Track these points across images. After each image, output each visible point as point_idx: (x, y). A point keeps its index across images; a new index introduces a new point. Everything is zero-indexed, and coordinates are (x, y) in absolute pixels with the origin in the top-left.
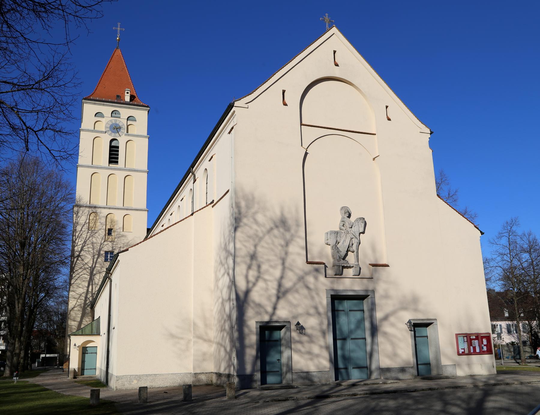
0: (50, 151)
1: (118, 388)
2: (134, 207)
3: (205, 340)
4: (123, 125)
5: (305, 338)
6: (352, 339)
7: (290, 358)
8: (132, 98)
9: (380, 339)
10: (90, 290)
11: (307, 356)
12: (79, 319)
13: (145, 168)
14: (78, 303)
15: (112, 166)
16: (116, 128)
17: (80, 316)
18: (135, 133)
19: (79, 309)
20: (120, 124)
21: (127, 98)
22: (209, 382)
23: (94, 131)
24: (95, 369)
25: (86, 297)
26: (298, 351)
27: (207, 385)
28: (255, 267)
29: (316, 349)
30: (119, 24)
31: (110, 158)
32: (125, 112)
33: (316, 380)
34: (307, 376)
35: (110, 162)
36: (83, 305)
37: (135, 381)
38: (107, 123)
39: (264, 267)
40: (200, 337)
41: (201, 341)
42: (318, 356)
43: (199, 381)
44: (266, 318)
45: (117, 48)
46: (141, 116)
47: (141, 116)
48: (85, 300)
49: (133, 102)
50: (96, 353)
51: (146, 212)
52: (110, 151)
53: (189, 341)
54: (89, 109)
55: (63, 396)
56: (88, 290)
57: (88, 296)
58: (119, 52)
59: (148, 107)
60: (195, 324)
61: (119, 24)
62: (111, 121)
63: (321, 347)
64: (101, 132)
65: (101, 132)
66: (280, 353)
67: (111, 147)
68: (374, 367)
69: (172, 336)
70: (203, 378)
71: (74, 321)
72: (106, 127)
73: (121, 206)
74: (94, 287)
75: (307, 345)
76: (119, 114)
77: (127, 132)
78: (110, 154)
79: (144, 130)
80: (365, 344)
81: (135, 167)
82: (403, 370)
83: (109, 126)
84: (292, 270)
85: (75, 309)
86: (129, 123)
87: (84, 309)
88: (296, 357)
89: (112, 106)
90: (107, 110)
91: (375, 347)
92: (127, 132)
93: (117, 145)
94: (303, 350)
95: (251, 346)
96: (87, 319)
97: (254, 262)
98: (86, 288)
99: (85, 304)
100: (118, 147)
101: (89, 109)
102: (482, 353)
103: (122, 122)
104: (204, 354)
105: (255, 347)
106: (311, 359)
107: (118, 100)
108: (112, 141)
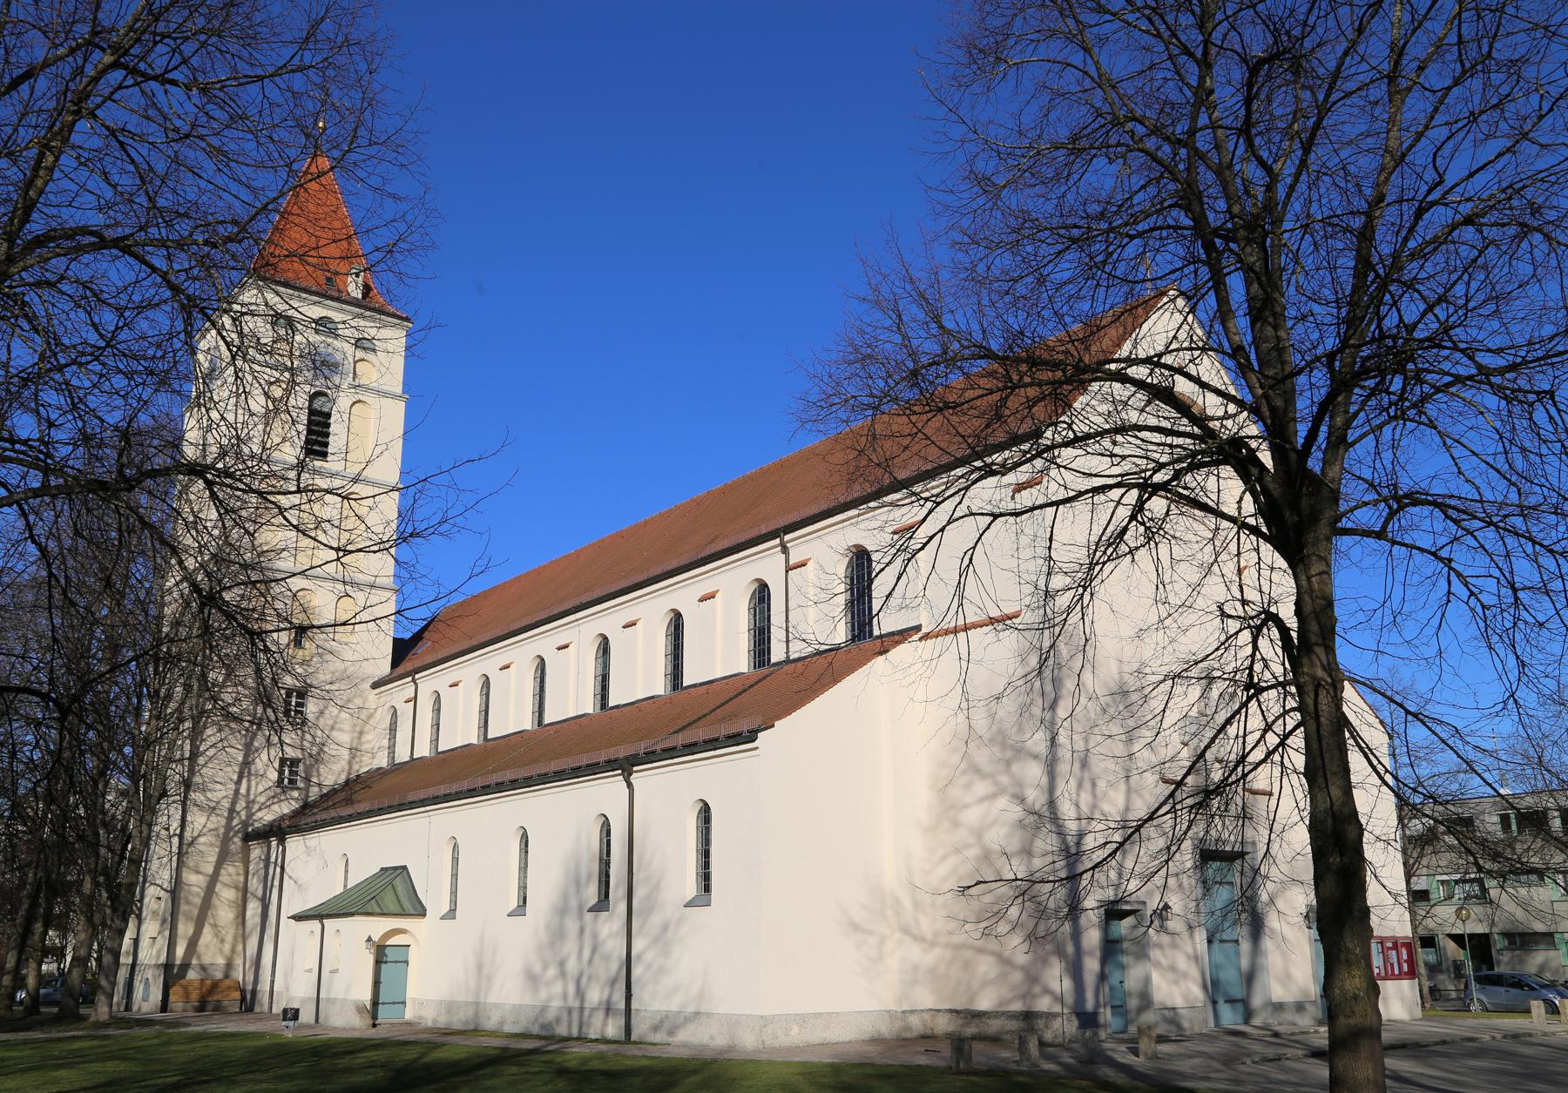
0: (1434, 554)
1: (768, 1043)
3: (915, 938)
5: (1165, 939)
6: (1222, 941)
7: (1147, 981)
9: (1267, 944)
10: (243, 790)
11: (1170, 976)
12: (210, 869)
14: (210, 826)
17: (213, 859)
19: (213, 840)
20: (338, 357)
22: (929, 1032)
24: (404, 1003)
25: (232, 811)
26: (1158, 964)
27: (924, 1037)
28: (1087, 785)
29: (1182, 963)
33: (1186, 1024)
34: (1171, 1016)
36: (222, 830)
37: (796, 1029)
39: (1101, 784)
40: (906, 931)
41: (908, 939)
42: (1185, 975)
43: (907, 1028)
44: (1110, 894)
46: (393, 339)
47: (393, 339)
48: (230, 819)
49: (366, 303)
50: (406, 962)
53: (883, 940)
55: (349, 1070)
56: (237, 792)
57: (238, 808)
59: (407, 319)
60: (897, 901)
63: (1189, 957)
66: (1122, 967)
68: (1257, 1001)
69: (855, 927)
70: (914, 1021)
71: (198, 872)
74: (253, 783)
75: (1168, 951)
79: (395, 384)
80: (1238, 954)
82: (1300, 1007)
84: (1140, 795)
85: (202, 840)
86: (360, 354)
87: (225, 842)
88: (1156, 978)
91: (1260, 960)
94: (1164, 961)
95: (1091, 953)
96: (231, 870)
97: (1086, 775)
98: (233, 786)
99: (228, 827)
100: (329, 415)
102: (1400, 977)
104: (915, 968)
105: (1098, 954)
106: (1176, 982)
108: (313, 397)
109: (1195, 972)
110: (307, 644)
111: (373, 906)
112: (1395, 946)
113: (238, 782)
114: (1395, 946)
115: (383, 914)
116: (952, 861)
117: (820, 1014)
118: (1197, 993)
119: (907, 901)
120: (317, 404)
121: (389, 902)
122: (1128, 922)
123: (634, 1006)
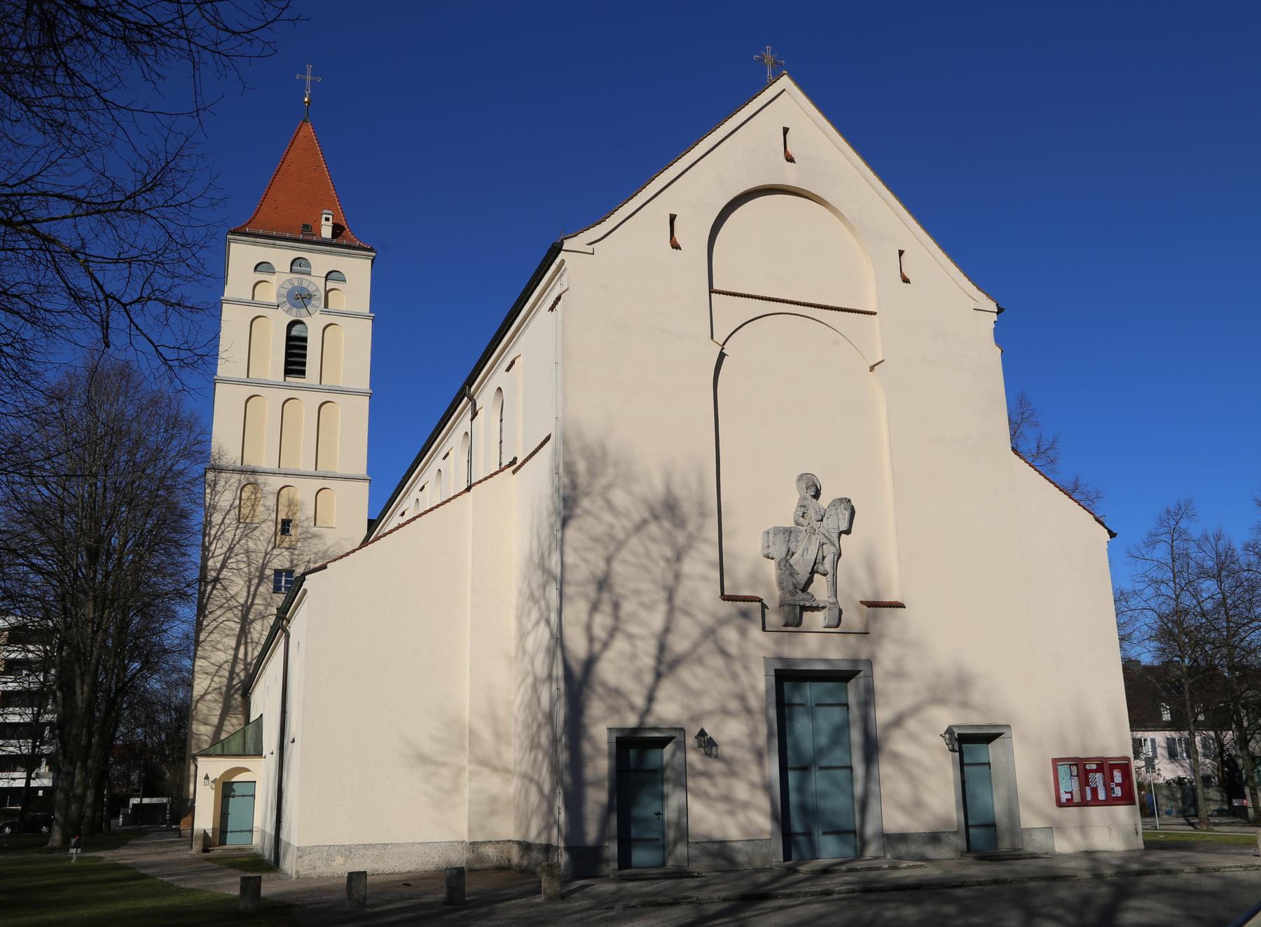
1: (302, 873)
2: (340, 471)
3: (495, 769)
4: (318, 290)
7: (684, 811)
8: (337, 230)
9: (885, 769)
10: (241, 655)
11: (721, 806)
12: (215, 720)
13: (364, 383)
15: (292, 380)
16: (301, 298)
18: (344, 308)
19: (217, 697)
20: (311, 289)
21: (326, 232)
22: (504, 863)
23: (252, 303)
24: (251, 831)
25: (232, 672)
26: (702, 795)
28: (606, 607)
29: (742, 791)
30: (309, 67)
31: (287, 363)
32: (321, 262)
34: (720, 850)
35: (288, 372)
36: (224, 689)
37: (340, 860)
38: (281, 287)
40: (483, 762)
42: (745, 805)
43: (481, 859)
44: (632, 721)
45: (305, 121)
46: (358, 270)
47: (358, 270)
48: (231, 679)
50: (253, 796)
51: (367, 484)
52: (288, 347)
53: (460, 770)
54: (243, 256)
55: (180, 891)
56: (236, 656)
57: (237, 670)
58: (308, 129)
59: (371, 250)
60: (472, 733)
61: (309, 67)
62: (290, 281)
63: (753, 785)
64: (269, 306)
65: (269, 306)
66: (663, 797)
67: (289, 338)
68: (870, 830)
69: (423, 759)
70: (491, 852)
71: (206, 724)
72: (279, 295)
73: (311, 469)
74: (250, 649)
76: (308, 265)
77: (326, 306)
78: (288, 355)
80: (851, 780)
81: (342, 384)
82: (934, 838)
83: (285, 292)
84: (688, 614)
85: (208, 697)
86: (330, 285)
89: (293, 248)
90: (281, 256)
91: (874, 787)
92: (326, 306)
93: (303, 335)
95: (597, 783)
96: (234, 721)
97: (606, 596)
98: (232, 652)
100: (305, 340)
101: (243, 256)
102: (1110, 801)
103: (316, 283)
104: (493, 800)
105: (606, 784)
106: (731, 813)
107: (306, 236)
108: (292, 325)
109: (763, 802)
110: (292, 532)
111: (218, 750)
112: (1100, 768)
113: (237, 648)
114: (1100, 768)
115: (222, 755)
116: (522, 689)
117: (372, 846)
118: (762, 822)
119: (486, 734)
120: (294, 332)
121: (235, 746)
122: (669, 749)
123: (284, 836)
